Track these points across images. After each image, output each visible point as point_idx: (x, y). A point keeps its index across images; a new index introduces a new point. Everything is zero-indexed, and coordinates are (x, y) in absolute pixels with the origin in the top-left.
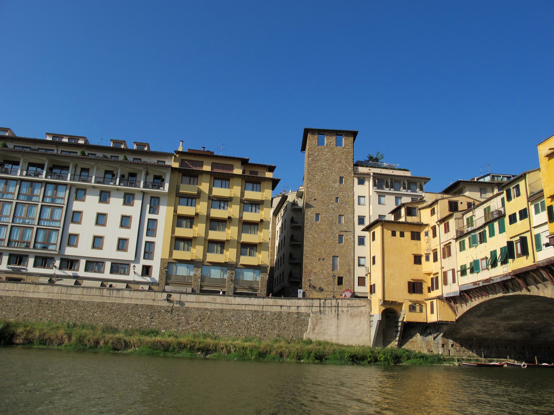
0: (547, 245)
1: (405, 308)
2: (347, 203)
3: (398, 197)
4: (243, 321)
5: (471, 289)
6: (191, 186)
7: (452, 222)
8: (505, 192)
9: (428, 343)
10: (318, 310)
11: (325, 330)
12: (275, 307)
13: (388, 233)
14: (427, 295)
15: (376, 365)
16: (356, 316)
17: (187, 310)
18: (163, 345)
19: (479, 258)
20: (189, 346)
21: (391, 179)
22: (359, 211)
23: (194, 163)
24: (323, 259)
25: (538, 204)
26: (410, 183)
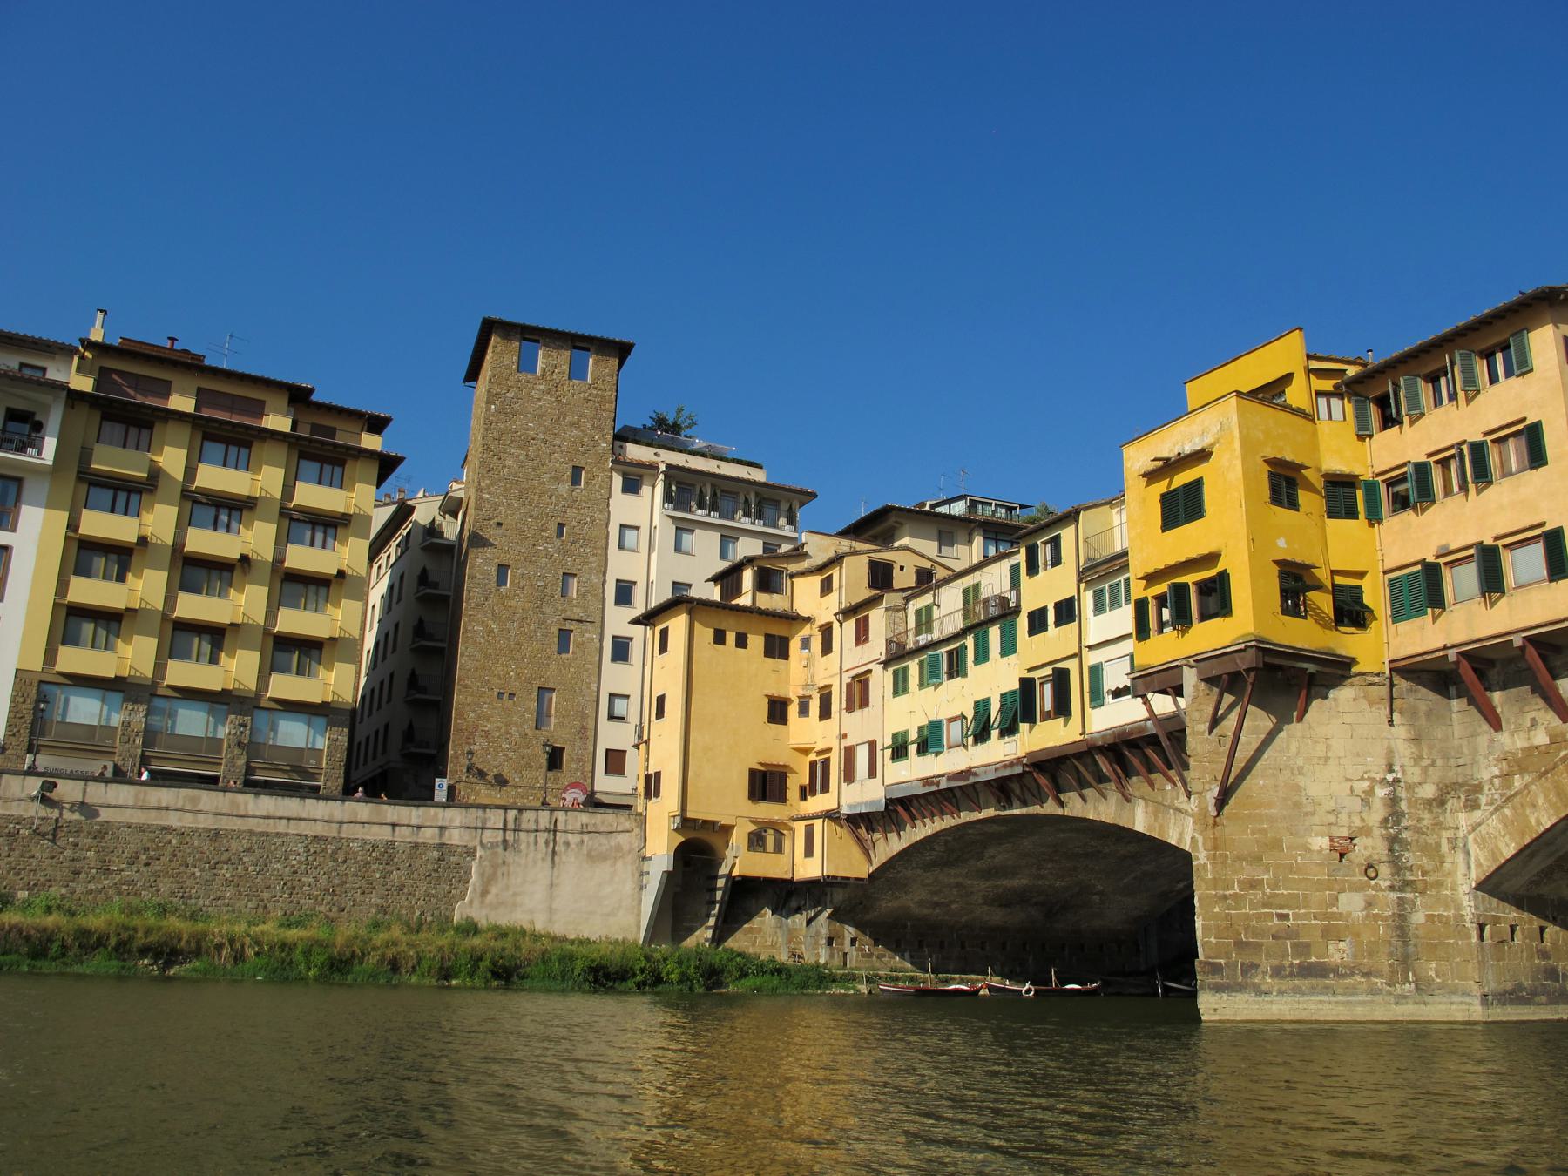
0: (1117, 693)
1: (738, 839)
2: (587, 541)
3: (728, 538)
4: (278, 866)
5: (917, 797)
6: (130, 453)
7: (877, 618)
8: (1023, 550)
9: (791, 936)
10: (500, 838)
11: (515, 894)
12: (375, 828)
13: (705, 634)
14: (796, 805)
15: (658, 994)
16: (603, 857)
17: (105, 830)
18: (28, 938)
19: (943, 715)
20: (113, 941)
21: (713, 486)
22: (620, 566)
23: (138, 382)
24: (512, 695)
25: (1102, 590)
26: (761, 501)
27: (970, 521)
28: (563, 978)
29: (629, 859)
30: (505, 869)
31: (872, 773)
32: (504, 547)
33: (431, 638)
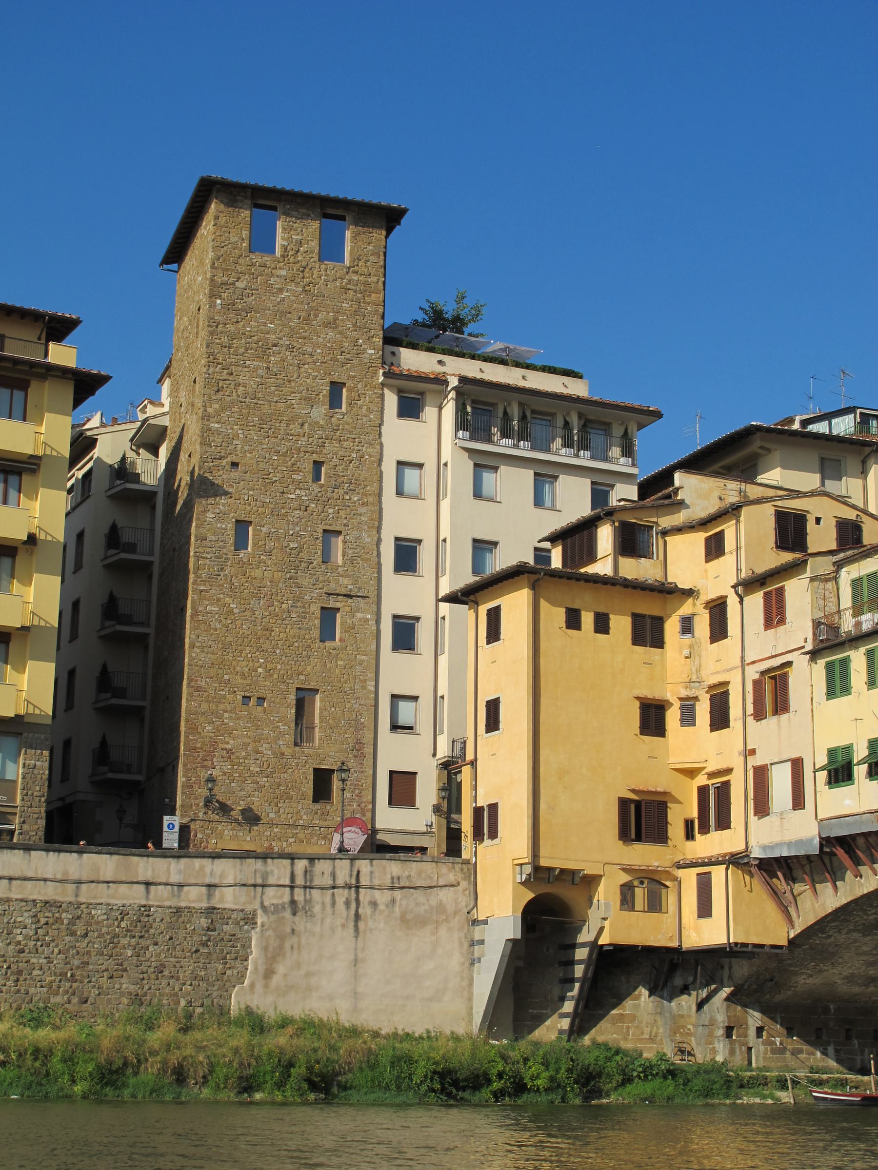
1: (606, 894)
2: (355, 485)
7: (798, 592)
9: (676, 1025)
10: (287, 899)
11: (308, 974)
12: (123, 888)
13: (554, 616)
14: (681, 848)
16: (421, 922)
21: (521, 405)
22: (400, 519)
24: (261, 700)
26: (586, 425)
27: (864, 444)
28: (399, 1088)
29: (455, 922)
30: (294, 939)
31: (798, 802)
32: (242, 496)
33: (128, 620)
